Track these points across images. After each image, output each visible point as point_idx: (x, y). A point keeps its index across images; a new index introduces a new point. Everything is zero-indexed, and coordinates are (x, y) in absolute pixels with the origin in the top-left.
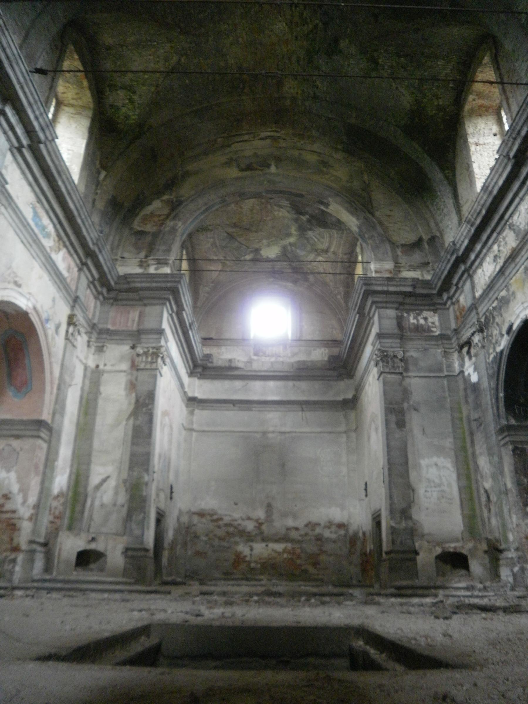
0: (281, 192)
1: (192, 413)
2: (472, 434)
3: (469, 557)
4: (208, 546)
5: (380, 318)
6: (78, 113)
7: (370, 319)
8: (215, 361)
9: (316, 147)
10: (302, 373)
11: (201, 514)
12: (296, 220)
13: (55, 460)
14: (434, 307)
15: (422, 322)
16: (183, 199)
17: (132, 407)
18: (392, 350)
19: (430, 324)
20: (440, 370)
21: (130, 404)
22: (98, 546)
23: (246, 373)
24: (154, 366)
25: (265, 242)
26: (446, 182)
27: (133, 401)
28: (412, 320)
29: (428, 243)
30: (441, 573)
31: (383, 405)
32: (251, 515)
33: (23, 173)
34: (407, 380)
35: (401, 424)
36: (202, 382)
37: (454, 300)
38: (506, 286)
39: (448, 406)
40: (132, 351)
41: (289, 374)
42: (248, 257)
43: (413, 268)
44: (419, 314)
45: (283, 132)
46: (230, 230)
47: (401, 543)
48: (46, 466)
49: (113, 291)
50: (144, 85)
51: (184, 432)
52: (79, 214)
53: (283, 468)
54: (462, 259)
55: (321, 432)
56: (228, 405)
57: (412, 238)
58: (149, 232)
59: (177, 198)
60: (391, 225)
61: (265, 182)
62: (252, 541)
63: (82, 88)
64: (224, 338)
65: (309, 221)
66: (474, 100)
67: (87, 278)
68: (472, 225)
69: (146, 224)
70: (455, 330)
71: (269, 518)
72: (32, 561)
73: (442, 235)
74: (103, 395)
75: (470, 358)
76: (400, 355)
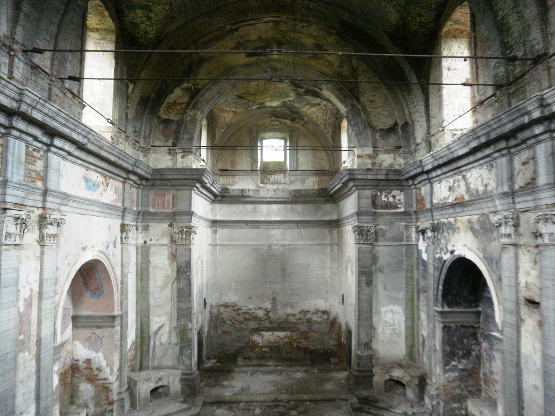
1: (215, 232)
4: (232, 327)
6: (103, 38)
8: (230, 192)
10: (297, 198)
11: (226, 306)
15: (391, 199)
16: (200, 86)
19: (397, 201)
21: (173, 270)
23: (255, 200)
27: (175, 269)
28: (384, 199)
29: (401, 128)
31: (357, 269)
34: (376, 248)
35: (369, 283)
39: (404, 267)
40: (171, 228)
41: (288, 200)
42: (254, 107)
43: (388, 152)
44: (389, 193)
45: (284, 17)
48: (121, 341)
53: (284, 271)
55: (312, 245)
56: (242, 224)
57: (389, 122)
58: (173, 121)
59: (194, 86)
61: (269, 69)
66: (451, 25)
69: (170, 113)
71: (274, 308)
72: (123, 407)
73: (413, 123)
74: (152, 264)
75: (424, 240)
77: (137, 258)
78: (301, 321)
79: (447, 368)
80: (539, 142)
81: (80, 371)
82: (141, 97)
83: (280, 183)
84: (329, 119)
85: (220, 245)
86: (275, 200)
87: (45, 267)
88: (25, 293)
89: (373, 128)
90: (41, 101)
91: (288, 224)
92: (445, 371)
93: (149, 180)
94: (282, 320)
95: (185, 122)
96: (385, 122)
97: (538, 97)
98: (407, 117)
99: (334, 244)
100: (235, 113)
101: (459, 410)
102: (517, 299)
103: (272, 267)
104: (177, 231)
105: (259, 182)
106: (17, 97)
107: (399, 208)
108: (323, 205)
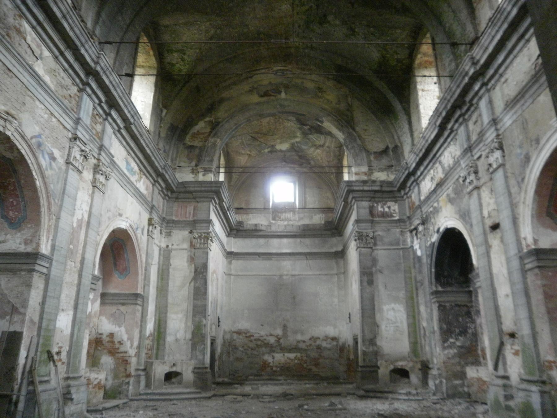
0: (289, 112)
1: (230, 263)
2: (417, 289)
3: (410, 373)
4: (244, 354)
5: (357, 208)
7: (351, 206)
8: (245, 226)
9: (313, 77)
10: (306, 232)
11: (239, 333)
12: (300, 129)
13: (147, 315)
14: (395, 199)
15: (387, 210)
16: (220, 120)
17: (193, 274)
18: (366, 231)
19: (392, 211)
20: (398, 244)
21: (191, 272)
22: (177, 369)
23: (267, 234)
24: (206, 245)
25: (278, 141)
26: (403, 112)
27: (193, 270)
28: (380, 209)
30: (393, 380)
32: (272, 333)
33: (120, 142)
34: (376, 251)
35: (371, 283)
36: (236, 240)
37: (408, 195)
38: (437, 201)
42: (266, 150)
43: (381, 170)
44: (384, 204)
45: (290, 67)
46: (253, 135)
47: (369, 361)
48: (142, 321)
49: (174, 193)
50: (191, 49)
51: (225, 277)
52: (153, 155)
53: (294, 300)
54: (413, 173)
57: (382, 147)
58: (196, 147)
59: (215, 119)
60: (367, 137)
61: (278, 106)
62: (274, 351)
63: (149, 55)
64: (250, 207)
65: (309, 129)
66: (421, 57)
67: (158, 189)
68: (417, 155)
70: (409, 217)
71: (285, 335)
72: (139, 382)
73: (402, 146)
74: (172, 266)
75: (417, 238)
76: (371, 235)
77: (159, 258)
78: (311, 348)
79: (446, 345)
80: (480, 98)
81: (103, 345)
82: (172, 124)
83: (291, 220)
84: (333, 160)
85: (234, 275)
86: (285, 234)
87: (94, 203)
88: (78, 215)
89: (368, 152)
90: (110, 69)
91: (298, 256)
92: (444, 348)
93: (174, 192)
94: (293, 347)
95: (206, 147)
96: (378, 146)
97: (470, 57)
98: (397, 141)
99: (340, 273)
100: (249, 155)
101: (461, 387)
102: (484, 231)
103: (282, 295)
104: (197, 236)
105: (271, 219)
106: (95, 59)
107: (394, 217)
108: (330, 239)
